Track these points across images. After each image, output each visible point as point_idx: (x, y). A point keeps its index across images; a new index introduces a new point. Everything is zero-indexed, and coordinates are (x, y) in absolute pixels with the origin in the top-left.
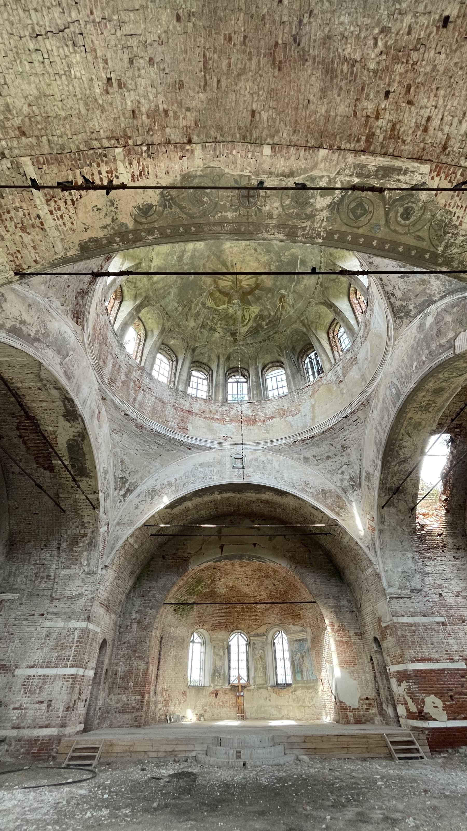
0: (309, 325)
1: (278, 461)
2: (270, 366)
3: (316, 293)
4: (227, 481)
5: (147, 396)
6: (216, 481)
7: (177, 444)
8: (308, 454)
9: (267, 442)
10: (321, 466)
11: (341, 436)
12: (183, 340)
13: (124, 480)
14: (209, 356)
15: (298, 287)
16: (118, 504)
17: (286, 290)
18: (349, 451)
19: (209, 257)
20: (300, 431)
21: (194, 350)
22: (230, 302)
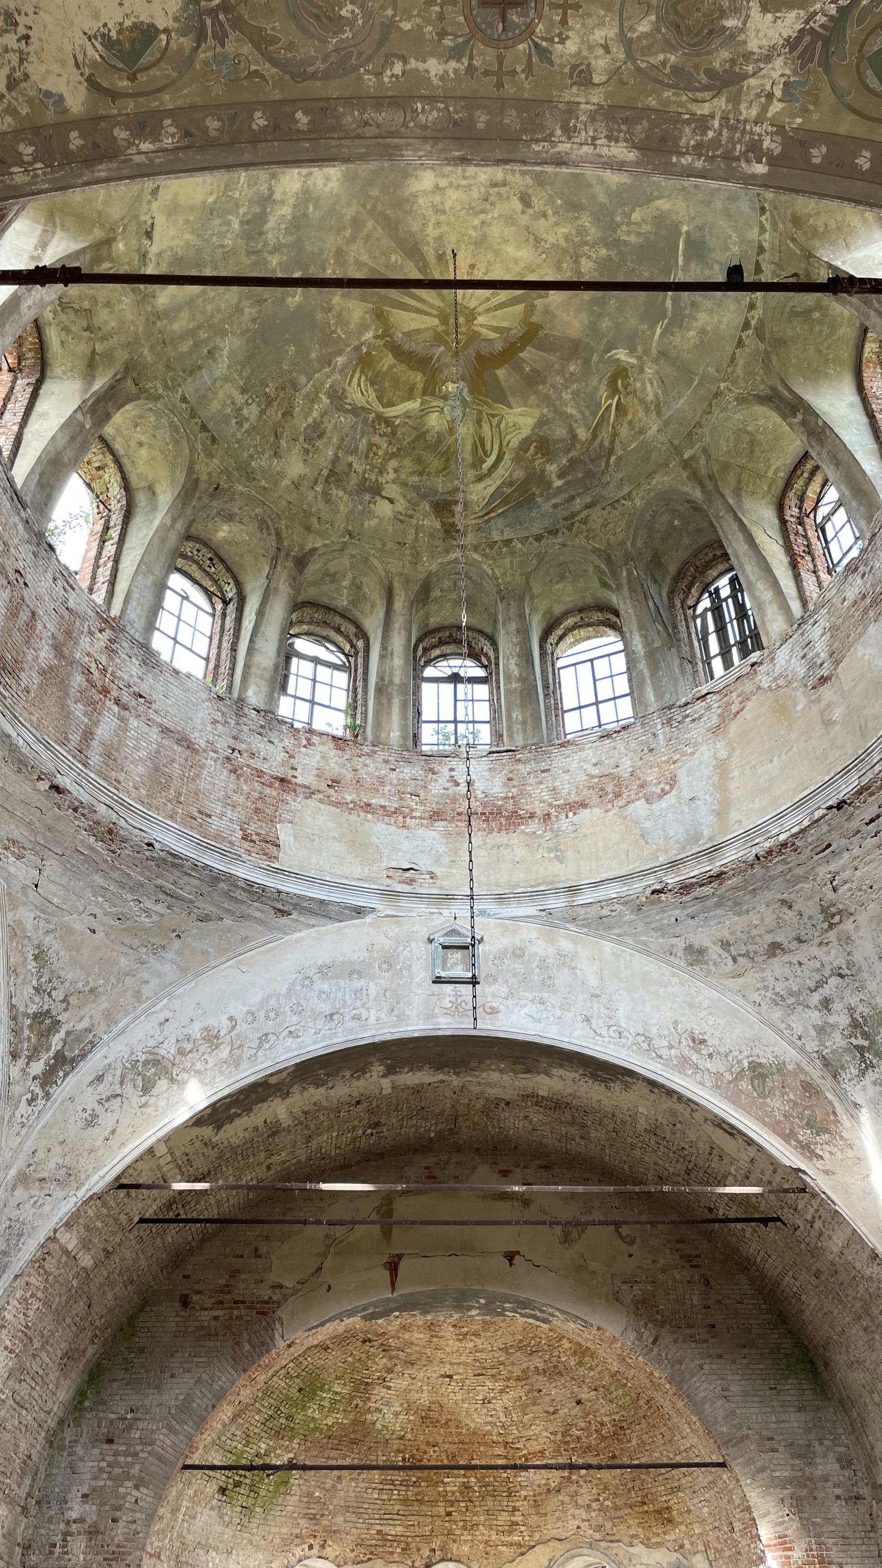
0: (711, 477)
1: (594, 958)
2: (570, 622)
3: (741, 362)
4: (414, 1027)
5: (133, 723)
7: (238, 894)
9: (557, 891)
11: (823, 872)
12: (263, 525)
13: (45, 1023)
14: (357, 586)
15: (676, 340)
16: (23, 1108)
17: (632, 350)
18: (848, 925)
19: (356, 223)
20: (673, 855)
21: (301, 563)
22: (431, 389)
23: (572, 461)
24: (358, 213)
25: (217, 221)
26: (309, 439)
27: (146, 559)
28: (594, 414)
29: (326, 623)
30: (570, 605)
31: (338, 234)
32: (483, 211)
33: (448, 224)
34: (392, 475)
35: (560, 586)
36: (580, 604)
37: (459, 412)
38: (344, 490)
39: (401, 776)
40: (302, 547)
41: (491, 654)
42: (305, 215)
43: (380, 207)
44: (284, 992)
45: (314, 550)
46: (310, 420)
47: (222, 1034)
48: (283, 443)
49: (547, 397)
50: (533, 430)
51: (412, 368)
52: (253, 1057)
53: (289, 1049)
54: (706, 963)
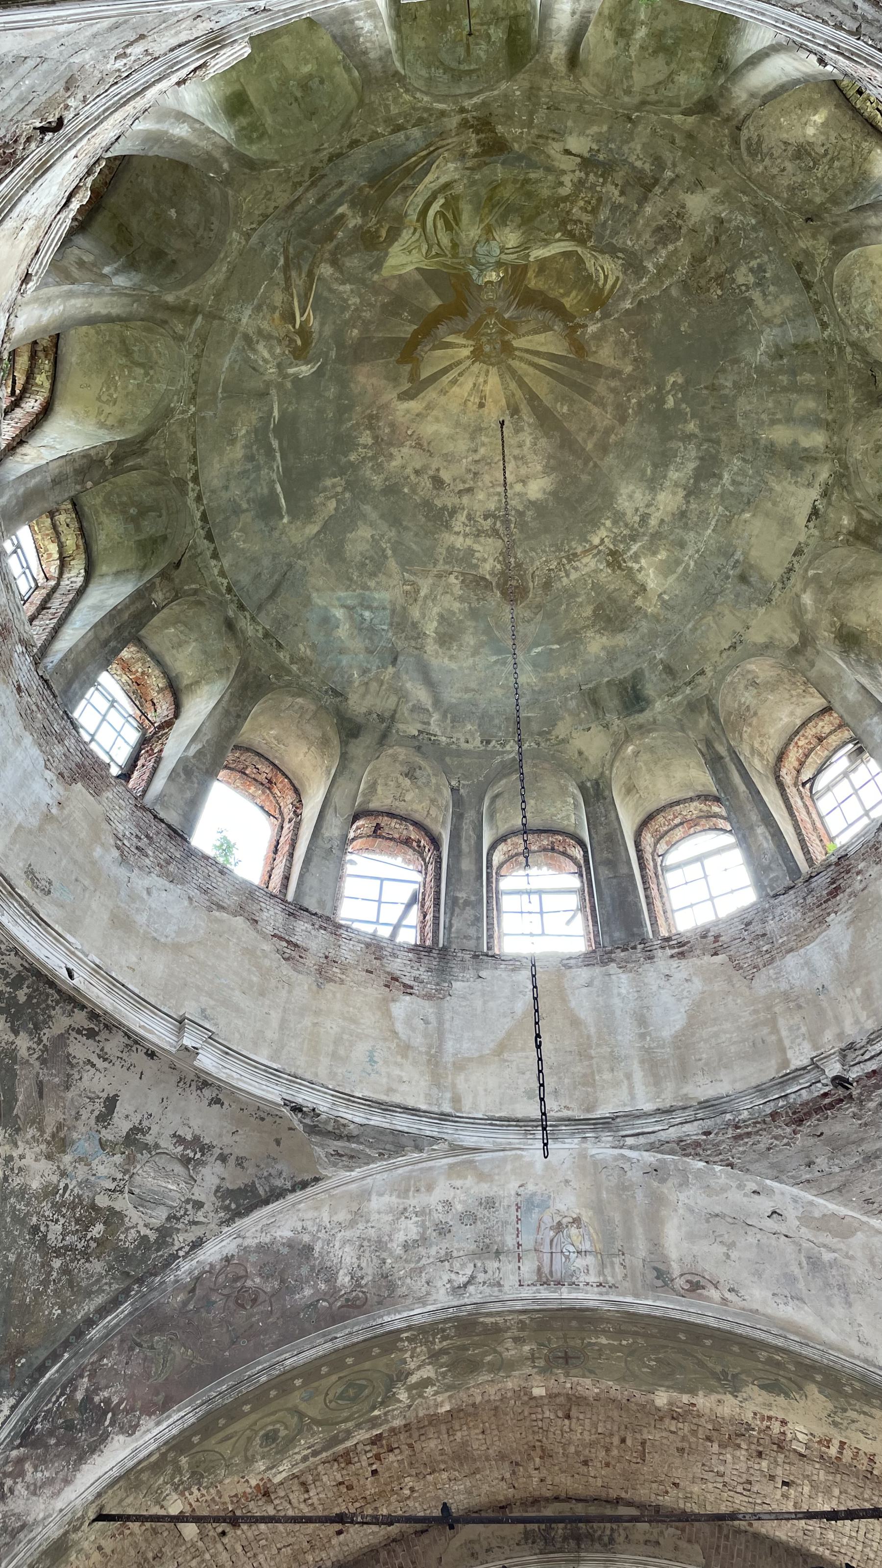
3: (186, 444)
12: (755, 149)
15: (254, 417)
17: (297, 380)
19: (603, 448)
21: (707, 106)
23: (331, 237)
25: (744, 489)
26: (676, 229)
28: (317, 297)
31: (623, 439)
32: (477, 462)
34: (567, 179)
35: (306, 69)
37: (481, 250)
38: (634, 168)
42: (655, 466)
43: (579, 463)
45: (687, 113)
46: (671, 247)
48: (709, 230)
50: (387, 254)
51: (541, 292)
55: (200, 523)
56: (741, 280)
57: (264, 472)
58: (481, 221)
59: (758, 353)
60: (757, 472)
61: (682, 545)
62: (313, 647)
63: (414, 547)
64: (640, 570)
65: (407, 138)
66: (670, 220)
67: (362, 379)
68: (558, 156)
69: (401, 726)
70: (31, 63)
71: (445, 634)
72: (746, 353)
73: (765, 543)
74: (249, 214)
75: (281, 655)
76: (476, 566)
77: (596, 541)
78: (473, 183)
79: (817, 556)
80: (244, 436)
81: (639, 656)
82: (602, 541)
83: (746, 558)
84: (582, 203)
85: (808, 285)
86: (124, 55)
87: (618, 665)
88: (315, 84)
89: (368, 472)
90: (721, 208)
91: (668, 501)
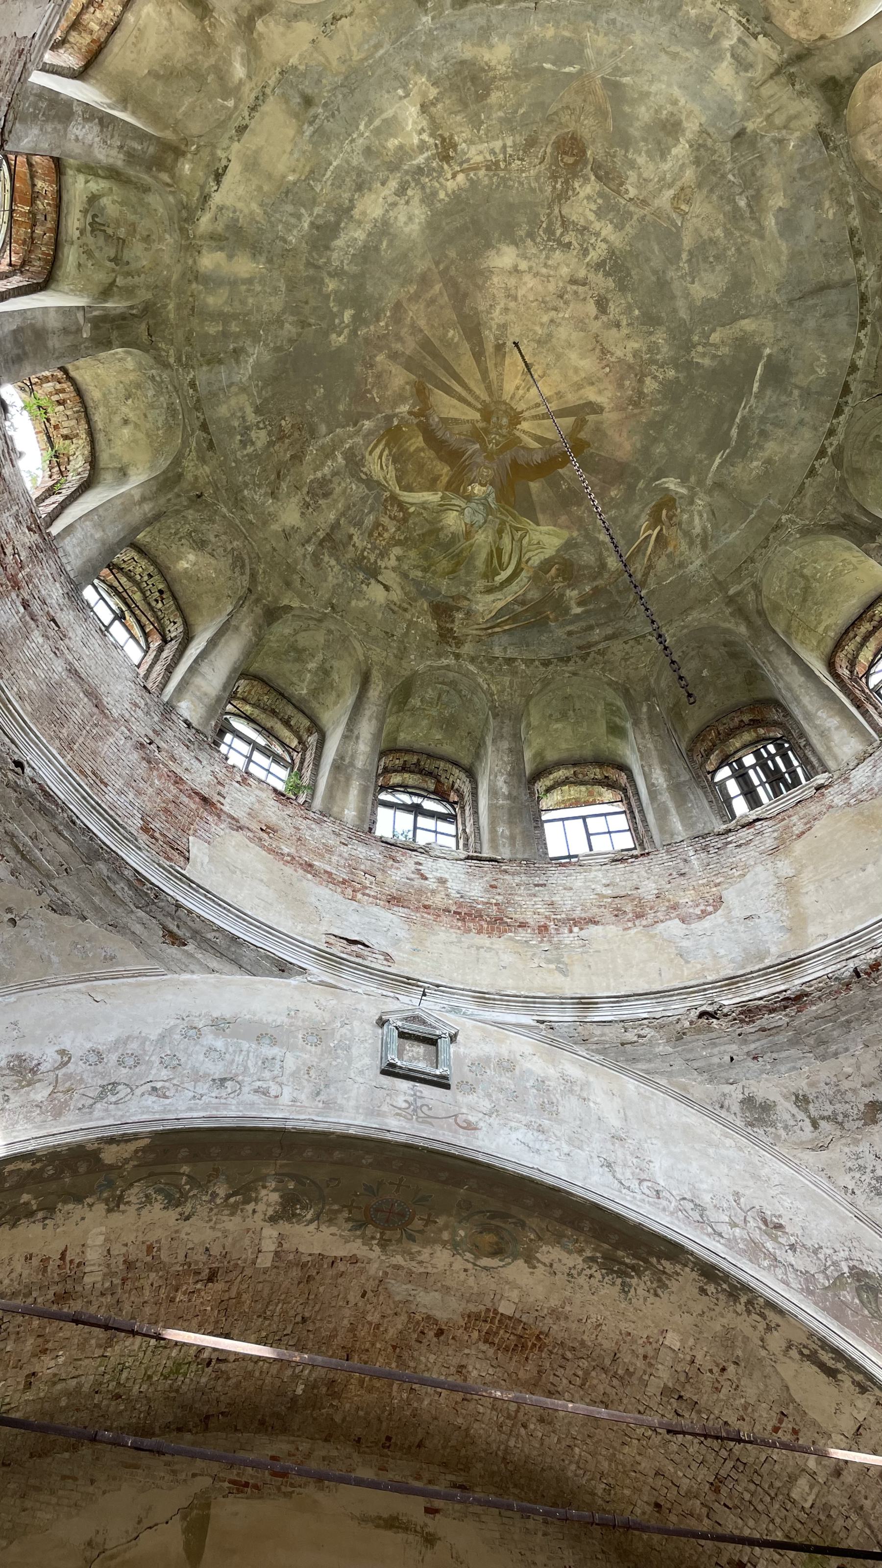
0: (761, 613)
1: (609, 1094)
2: (561, 774)
3: (810, 492)
5: (37, 637)
6: (291, 1105)
7: (120, 888)
8: (768, 1087)
10: (839, 1152)
12: (238, 562)
14: (325, 671)
15: (737, 470)
17: (684, 480)
19: (424, 281)
21: (272, 614)
22: (456, 486)
23: (596, 591)
24: (429, 269)
25: (289, 208)
27: (101, 511)
28: (630, 543)
29: (273, 713)
30: (565, 755)
31: (403, 286)
32: (555, 309)
33: (516, 313)
34: (393, 562)
35: (559, 726)
36: (577, 754)
37: (480, 518)
38: (338, 560)
39: (354, 852)
40: (276, 599)
41: (466, 789)
42: (377, 249)
43: (453, 272)
44: (153, 1037)
45: (288, 608)
46: (319, 474)
47: (42, 1068)
48: (284, 486)
49: (580, 519)
50: (558, 551)
51: (441, 458)
52: (86, 1110)
53: (147, 1110)
54: (773, 1125)
55: (846, 409)
56: (263, 434)
57: (760, 412)
58: (472, 545)
59: (257, 355)
60: (273, 226)
61: (368, 152)
62: (819, 205)
63: (656, 248)
64: (421, 131)
65: (505, 649)
66: (316, 502)
67: (627, 446)
68: (395, 586)
69: (774, 56)
70: (696, 1065)
71: (669, 134)
72: (267, 357)
73: (276, 141)
74: (648, 651)
75: (856, 223)
76: (601, 194)
77: (461, 177)
78: (468, 584)
79: (222, 125)
80: (757, 459)
81: (452, 26)
82: (454, 176)
83: (301, 127)
84: (386, 535)
85: (204, 427)
86: (639, 1036)
87: (481, 21)
88: (557, 715)
89: (665, 350)
90: (272, 509)
91: (372, 206)
